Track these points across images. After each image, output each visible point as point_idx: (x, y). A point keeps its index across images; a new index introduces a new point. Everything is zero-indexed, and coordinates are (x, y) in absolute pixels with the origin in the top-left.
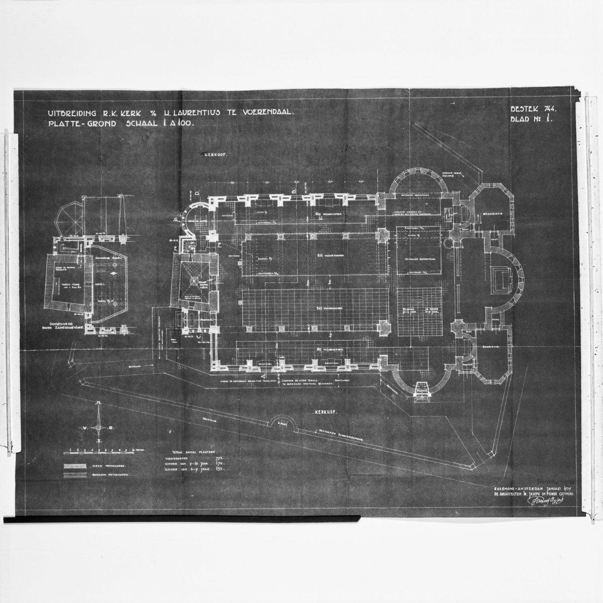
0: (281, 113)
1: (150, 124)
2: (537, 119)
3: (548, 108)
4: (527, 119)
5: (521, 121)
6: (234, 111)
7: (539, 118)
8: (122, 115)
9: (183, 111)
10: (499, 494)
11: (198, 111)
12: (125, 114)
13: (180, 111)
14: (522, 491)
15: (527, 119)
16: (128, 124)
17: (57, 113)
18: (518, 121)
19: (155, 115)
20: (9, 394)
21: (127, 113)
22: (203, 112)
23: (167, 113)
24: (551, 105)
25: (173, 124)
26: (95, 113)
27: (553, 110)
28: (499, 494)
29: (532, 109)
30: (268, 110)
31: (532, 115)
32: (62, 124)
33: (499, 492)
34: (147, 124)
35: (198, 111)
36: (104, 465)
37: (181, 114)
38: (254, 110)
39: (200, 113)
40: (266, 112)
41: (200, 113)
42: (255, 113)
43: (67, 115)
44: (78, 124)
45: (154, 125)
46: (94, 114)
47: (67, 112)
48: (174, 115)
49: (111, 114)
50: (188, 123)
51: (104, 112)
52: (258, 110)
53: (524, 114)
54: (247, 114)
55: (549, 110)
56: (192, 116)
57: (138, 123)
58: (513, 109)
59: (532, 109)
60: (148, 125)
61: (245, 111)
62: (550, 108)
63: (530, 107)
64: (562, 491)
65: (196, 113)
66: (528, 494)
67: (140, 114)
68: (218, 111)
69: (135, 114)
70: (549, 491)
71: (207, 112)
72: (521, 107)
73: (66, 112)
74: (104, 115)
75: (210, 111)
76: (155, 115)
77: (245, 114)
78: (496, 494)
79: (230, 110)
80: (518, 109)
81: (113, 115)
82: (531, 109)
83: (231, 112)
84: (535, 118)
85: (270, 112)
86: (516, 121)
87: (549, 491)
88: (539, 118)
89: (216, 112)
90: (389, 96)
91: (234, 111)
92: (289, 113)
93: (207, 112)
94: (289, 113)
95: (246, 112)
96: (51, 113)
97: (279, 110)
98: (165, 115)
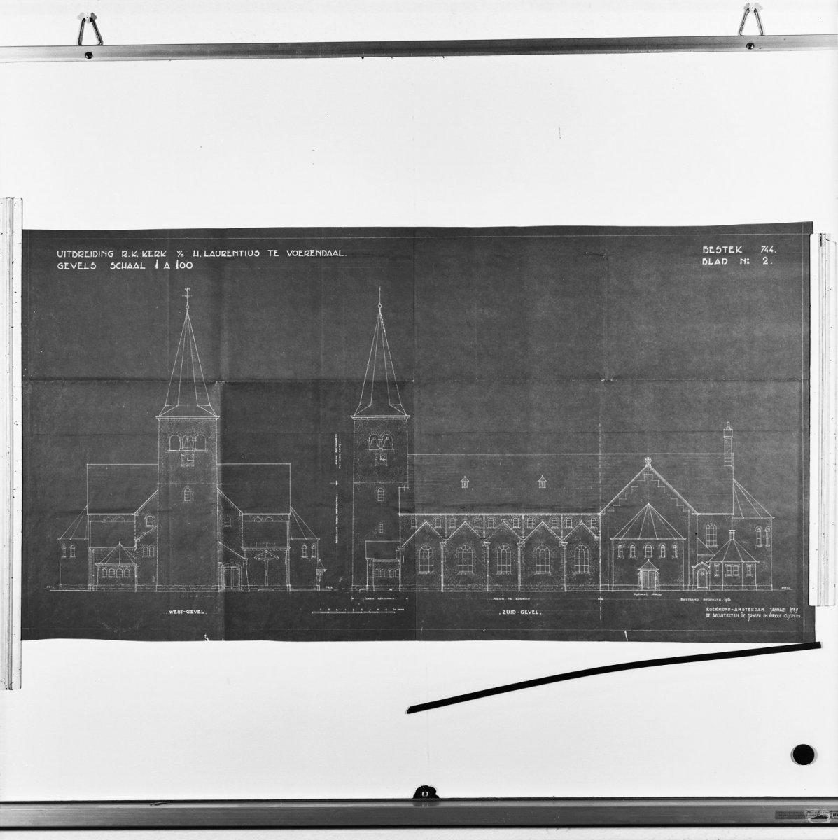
2: (745, 261)
4: (725, 261)
6: (275, 251)
8: (143, 255)
10: (711, 616)
12: (147, 254)
15: (725, 261)
16: (113, 266)
17: (67, 253)
19: (182, 255)
22: (239, 253)
23: (196, 254)
27: (772, 251)
28: (762, 616)
33: (711, 613)
36: (376, 600)
38: (300, 252)
43: (223, 255)
45: (141, 268)
46: (110, 255)
47: (79, 252)
48: (205, 256)
51: (123, 252)
55: (767, 251)
58: (706, 250)
61: (290, 252)
62: (769, 249)
63: (731, 248)
64: (788, 612)
65: (231, 254)
66: (747, 615)
67: (740, 250)
68: (256, 251)
69: (160, 255)
70: (773, 613)
71: (243, 253)
72: (718, 248)
74: (123, 256)
76: (182, 255)
77: (289, 255)
78: (708, 615)
79: (270, 251)
81: (133, 255)
84: (741, 260)
86: (709, 264)
87: (773, 613)
89: (254, 252)
90: (645, 237)
91: (275, 251)
96: (60, 254)
98: (194, 255)
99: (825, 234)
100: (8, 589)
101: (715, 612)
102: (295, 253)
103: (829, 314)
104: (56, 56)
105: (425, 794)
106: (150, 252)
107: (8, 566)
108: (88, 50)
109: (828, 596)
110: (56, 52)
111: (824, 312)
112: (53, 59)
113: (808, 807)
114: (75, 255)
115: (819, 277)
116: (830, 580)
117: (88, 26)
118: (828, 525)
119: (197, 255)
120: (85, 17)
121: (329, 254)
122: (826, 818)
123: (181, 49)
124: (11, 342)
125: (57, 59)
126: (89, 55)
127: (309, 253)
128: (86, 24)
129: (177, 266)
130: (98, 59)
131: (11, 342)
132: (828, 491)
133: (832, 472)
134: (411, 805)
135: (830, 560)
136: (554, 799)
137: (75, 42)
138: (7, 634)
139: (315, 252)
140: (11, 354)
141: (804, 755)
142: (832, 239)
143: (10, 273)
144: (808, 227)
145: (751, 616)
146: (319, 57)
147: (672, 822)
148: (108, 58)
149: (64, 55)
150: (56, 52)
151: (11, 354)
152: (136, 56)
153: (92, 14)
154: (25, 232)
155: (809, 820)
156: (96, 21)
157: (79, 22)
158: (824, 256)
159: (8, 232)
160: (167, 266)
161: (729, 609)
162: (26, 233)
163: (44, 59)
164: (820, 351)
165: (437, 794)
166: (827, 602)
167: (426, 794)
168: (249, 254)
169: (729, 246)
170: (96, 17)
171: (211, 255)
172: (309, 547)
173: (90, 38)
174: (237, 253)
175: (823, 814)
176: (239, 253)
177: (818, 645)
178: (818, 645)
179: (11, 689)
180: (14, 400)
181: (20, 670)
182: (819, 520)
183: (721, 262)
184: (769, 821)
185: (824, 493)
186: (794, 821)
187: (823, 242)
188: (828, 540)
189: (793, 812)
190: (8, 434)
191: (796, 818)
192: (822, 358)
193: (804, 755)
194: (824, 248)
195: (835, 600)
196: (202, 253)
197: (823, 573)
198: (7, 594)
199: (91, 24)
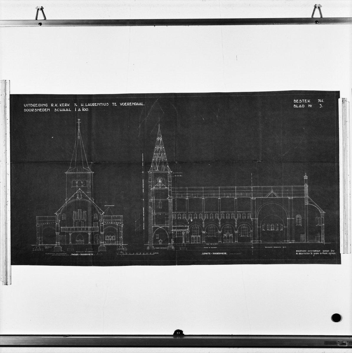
1: (67, 110)
6: (115, 103)
7: (311, 105)
10: (298, 253)
11: (132, 103)
12: (62, 105)
13: (89, 104)
14: (310, 252)
15: (303, 106)
16: (55, 110)
17: (28, 105)
21: (63, 105)
22: (100, 104)
23: (82, 105)
24: (321, 99)
25: (79, 110)
28: (298, 253)
30: (132, 103)
33: (298, 252)
34: (65, 110)
38: (126, 103)
40: (131, 104)
42: (46, 110)
43: (93, 105)
44: (116, 105)
48: (86, 106)
49: (55, 105)
50: (87, 110)
51: (52, 104)
52: (128, 103)
55: (321, 101)
56: (129, 106)
57: (61, 110)
58: (295, 101)
60: (66, 110)
63: (306, 100)
64: (330, 252)
65: (97, 105)
66: (313, 254)
68: (107, 103)
69: (67, 105)
70: (324, 252)
71: (102, 104)
74: (52, 106)
76: (77, 106)
78: (297, 254)
79: (113, 103)
81: (56, 106)
84: (309, 105)
85: (133, 104)
87: (324, 252)
88: (311, 105)
89: (106, 104)
91: (115, 103)
93: (102, 104)
97: (138, 103)
98: (81, 105)
99: (344, 98)
100: (5, 243)
101: (300, 252)
102: (123, 104)
103: (347, 132)
104: (27, 24)
105: (178, 333)
106: (63, 104)
107: (5, 234)
108: (40, 22)
109: (348, 249)
110: (26, 23)
111: (344, 130)
112: (25, 26)
113: (338, 340)
114: (32, 105)
115: (342, 116)
116: (348, 243)
117: (40, 12)
118: (347, 220)
119: (83, 105)
120: (39, 8)
121: (137, 104)
122: (345, 344)
123: (78, 22)
124: (6, 140)
125: (27, 26)
126: (40, 24)
127: (129, 104)
128: (39, 11)
130: (44, 25)
131: (6, 140)
132: (347, 205)
133: (349, 198)
134: (172, 338)
135: (348, 234)
136: (232, 336)
137: (35, 19)
138: (5, 262)
139: (132, 103)
140: (6, 145)
141: (336, 318)
142: (348, 100)
143: (5, 111)
144: (337, 94)
145: (314, 254)
146: (136, 26)
147: (281, 345)
148: (48, 25)
149: (30, 24)
150: (26, 23)
151: (6, 145)
152: (60, 24)
153: (42, 7)
154: (11, 95)
155: (339, 345)
156: (43, 10)
157: (36, 10)
158: (344, 107)
159: (4, 94)
161: (306, 251)
162: (12, 96)
163: (22, 26)
164: (343, 147)
165: (183, 333)
166: (348, 252)
167: (179, 333)
168: (104, 105)
169: (305, 99)
170: (43, 8)
171: (88, 105)
173: (41, 17)
174: (99, 104)
175: (344, 343)
176: (100, 104)
179: (7, 285)
180: (7, 164)
181: (11, 277)
182: (343, 218)
183: (302, 106)
184: (322, 345)
185: (346, 206)
186: (332, 345)
187: (344, 102)
188: (347, 226)
189: (332, 342)
190: (5, 179)
191: (333, 344)
192: (344, 150)
193: (336, 318)
194: (344, 104)
195: (351, 251)
196: (84, 105)
197: (345, 240)
198: (5, 245)
199: (41, 11)
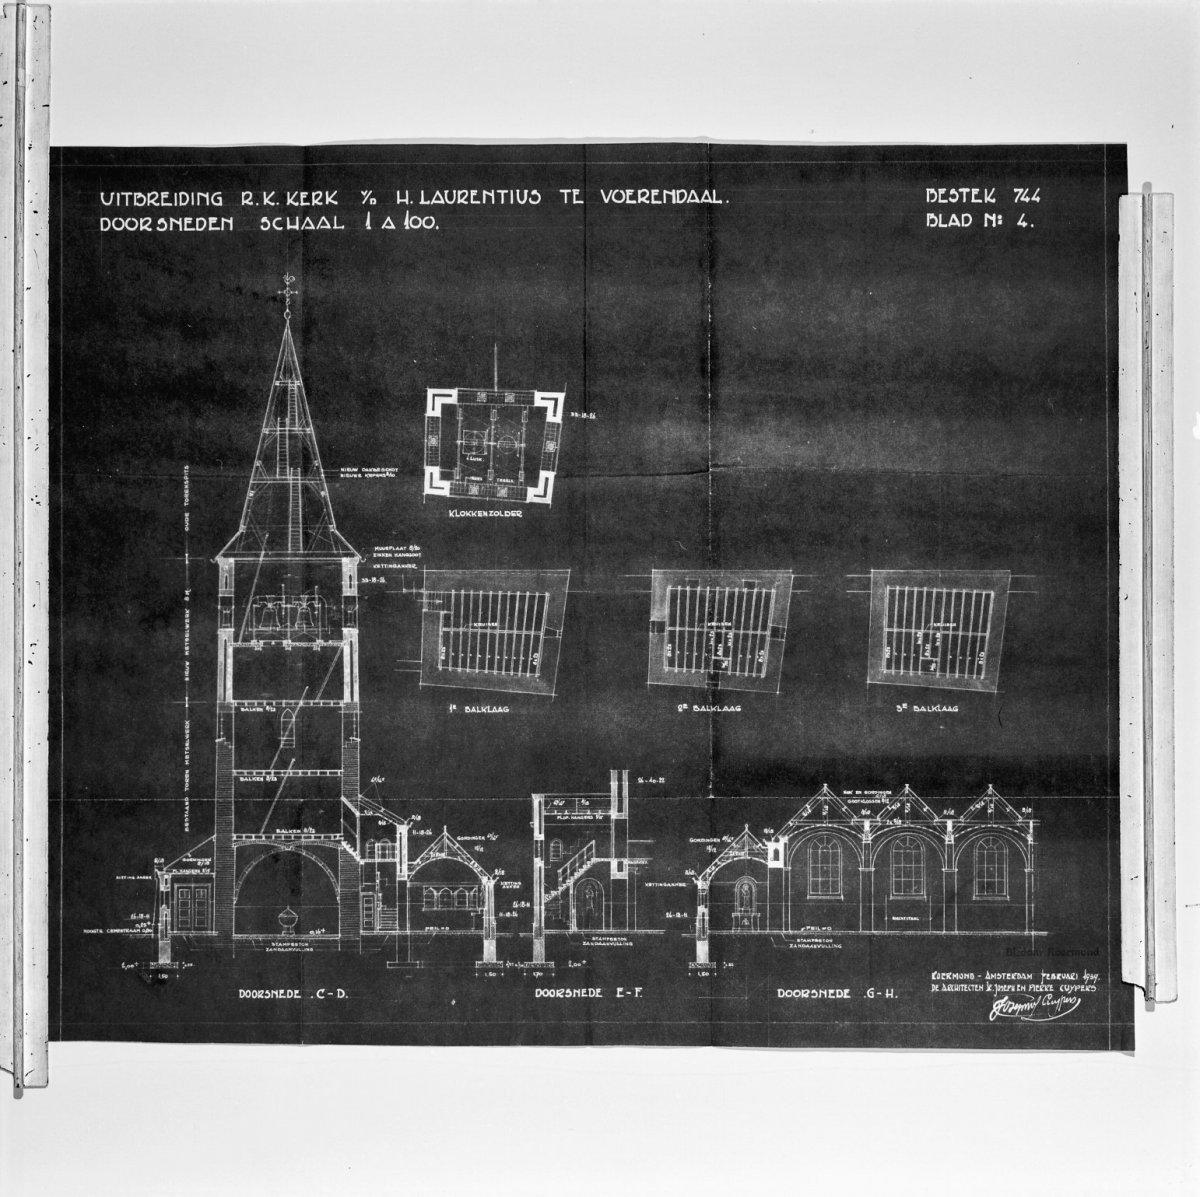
0: (697, 200)
3: (1021, 194)
4: (967, 220)
5: (951, 224)
6: (576, 192)
9: (446, 192)
12: (297, 199)
15: (967, 220)
16: (265, 225)
17: (123, 198)
18: (946, 226)
19: (373, 201)
20: (19, 475)
22: (498, 196)
26: (220, 198)
29: (980, 196)
31: (979, 211)
32: (388, 224)
35: (485, 192)
37: (442, 202)
38: (630, 192)
39: (489, 198)
40: (659, 197)
41: (489, 198)
45: (335, 227)
46: (217, 201)
48: (422, 202)
50: (429, 222)
51: (243, 194)
53: (959, 208)
54: (611, 199)
56: (160, 207)
59: (980, 196)
62: (1030, 195)
63: (975, 191)
65: (478, 197)
66: (993, 988)
67: (271, 200)
68: (534, 192)
69: (323, 199)
71: (507, 196)
73: (146, 196)
75: (515, 193)
77: (606, 201)
78: (935, 988)
79: (566, 191)
80: (944, 197)
81: (266, 201)
82: (977, 197)
83: (570, 195)
84: (987, 216)
86: (941, 225)
89: (529, 195)
92: (717, 199)
93: (507, 196)
94: (717, 199)
95: (608, 197)
96: (107, 199)
98: (399, 201)
114: (140, 200)
129: (406, 223)
139: (661, 194)
160: (388, 224)
172: (208, 867)
176: (498, 196)
177: (18, 1095)
178: (18, 1095)
